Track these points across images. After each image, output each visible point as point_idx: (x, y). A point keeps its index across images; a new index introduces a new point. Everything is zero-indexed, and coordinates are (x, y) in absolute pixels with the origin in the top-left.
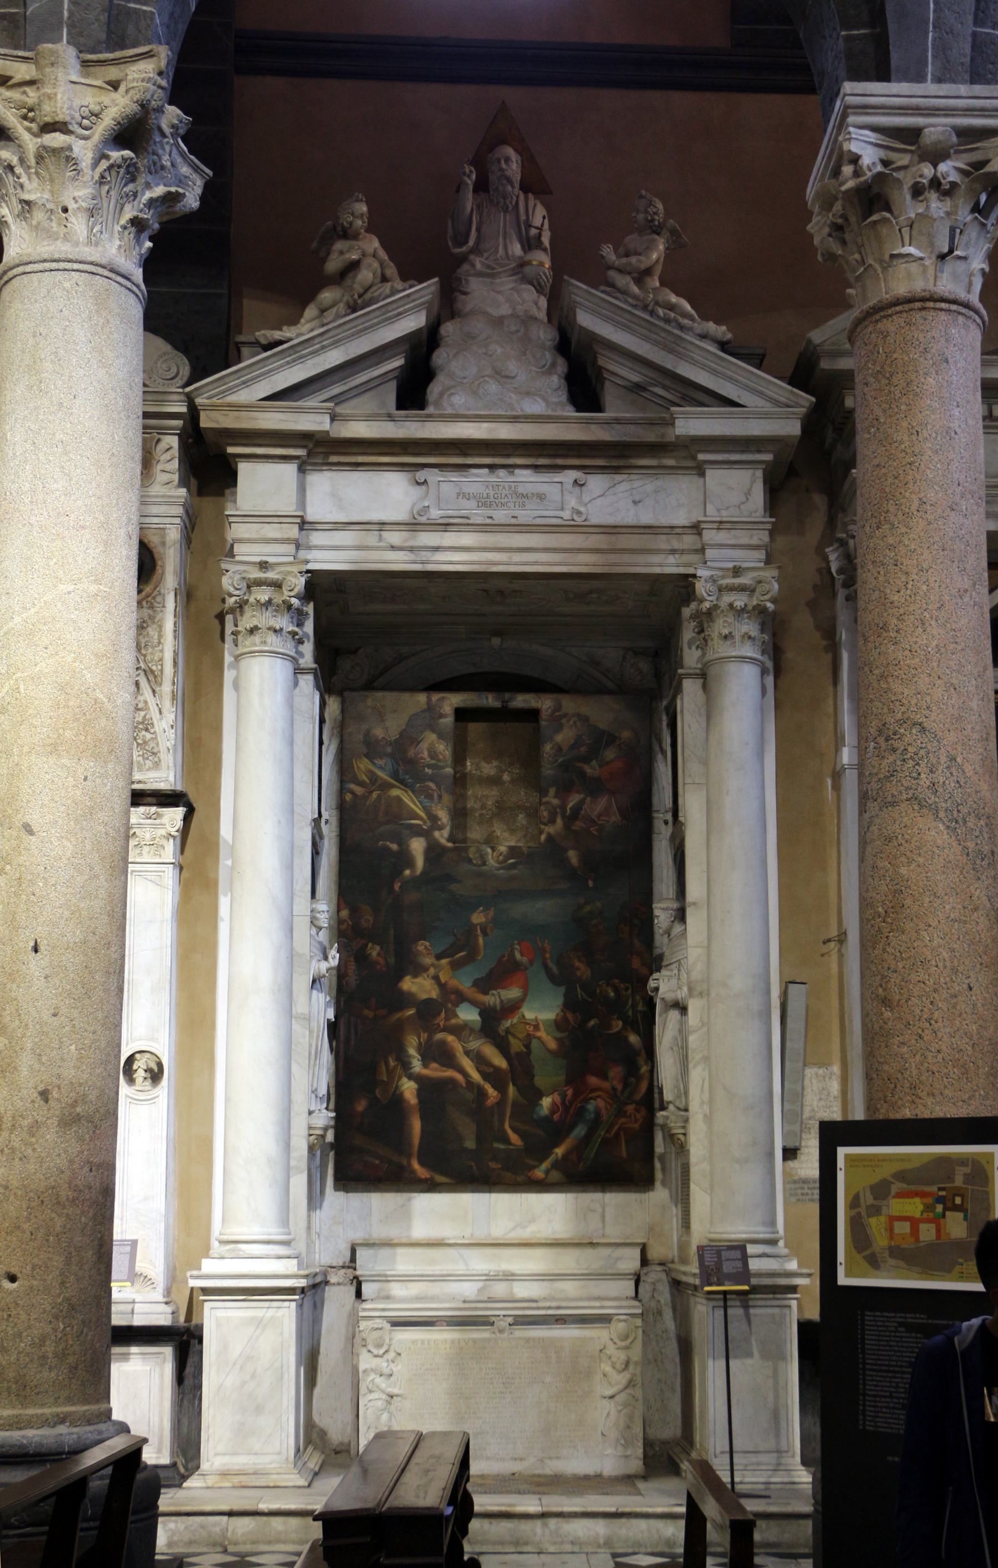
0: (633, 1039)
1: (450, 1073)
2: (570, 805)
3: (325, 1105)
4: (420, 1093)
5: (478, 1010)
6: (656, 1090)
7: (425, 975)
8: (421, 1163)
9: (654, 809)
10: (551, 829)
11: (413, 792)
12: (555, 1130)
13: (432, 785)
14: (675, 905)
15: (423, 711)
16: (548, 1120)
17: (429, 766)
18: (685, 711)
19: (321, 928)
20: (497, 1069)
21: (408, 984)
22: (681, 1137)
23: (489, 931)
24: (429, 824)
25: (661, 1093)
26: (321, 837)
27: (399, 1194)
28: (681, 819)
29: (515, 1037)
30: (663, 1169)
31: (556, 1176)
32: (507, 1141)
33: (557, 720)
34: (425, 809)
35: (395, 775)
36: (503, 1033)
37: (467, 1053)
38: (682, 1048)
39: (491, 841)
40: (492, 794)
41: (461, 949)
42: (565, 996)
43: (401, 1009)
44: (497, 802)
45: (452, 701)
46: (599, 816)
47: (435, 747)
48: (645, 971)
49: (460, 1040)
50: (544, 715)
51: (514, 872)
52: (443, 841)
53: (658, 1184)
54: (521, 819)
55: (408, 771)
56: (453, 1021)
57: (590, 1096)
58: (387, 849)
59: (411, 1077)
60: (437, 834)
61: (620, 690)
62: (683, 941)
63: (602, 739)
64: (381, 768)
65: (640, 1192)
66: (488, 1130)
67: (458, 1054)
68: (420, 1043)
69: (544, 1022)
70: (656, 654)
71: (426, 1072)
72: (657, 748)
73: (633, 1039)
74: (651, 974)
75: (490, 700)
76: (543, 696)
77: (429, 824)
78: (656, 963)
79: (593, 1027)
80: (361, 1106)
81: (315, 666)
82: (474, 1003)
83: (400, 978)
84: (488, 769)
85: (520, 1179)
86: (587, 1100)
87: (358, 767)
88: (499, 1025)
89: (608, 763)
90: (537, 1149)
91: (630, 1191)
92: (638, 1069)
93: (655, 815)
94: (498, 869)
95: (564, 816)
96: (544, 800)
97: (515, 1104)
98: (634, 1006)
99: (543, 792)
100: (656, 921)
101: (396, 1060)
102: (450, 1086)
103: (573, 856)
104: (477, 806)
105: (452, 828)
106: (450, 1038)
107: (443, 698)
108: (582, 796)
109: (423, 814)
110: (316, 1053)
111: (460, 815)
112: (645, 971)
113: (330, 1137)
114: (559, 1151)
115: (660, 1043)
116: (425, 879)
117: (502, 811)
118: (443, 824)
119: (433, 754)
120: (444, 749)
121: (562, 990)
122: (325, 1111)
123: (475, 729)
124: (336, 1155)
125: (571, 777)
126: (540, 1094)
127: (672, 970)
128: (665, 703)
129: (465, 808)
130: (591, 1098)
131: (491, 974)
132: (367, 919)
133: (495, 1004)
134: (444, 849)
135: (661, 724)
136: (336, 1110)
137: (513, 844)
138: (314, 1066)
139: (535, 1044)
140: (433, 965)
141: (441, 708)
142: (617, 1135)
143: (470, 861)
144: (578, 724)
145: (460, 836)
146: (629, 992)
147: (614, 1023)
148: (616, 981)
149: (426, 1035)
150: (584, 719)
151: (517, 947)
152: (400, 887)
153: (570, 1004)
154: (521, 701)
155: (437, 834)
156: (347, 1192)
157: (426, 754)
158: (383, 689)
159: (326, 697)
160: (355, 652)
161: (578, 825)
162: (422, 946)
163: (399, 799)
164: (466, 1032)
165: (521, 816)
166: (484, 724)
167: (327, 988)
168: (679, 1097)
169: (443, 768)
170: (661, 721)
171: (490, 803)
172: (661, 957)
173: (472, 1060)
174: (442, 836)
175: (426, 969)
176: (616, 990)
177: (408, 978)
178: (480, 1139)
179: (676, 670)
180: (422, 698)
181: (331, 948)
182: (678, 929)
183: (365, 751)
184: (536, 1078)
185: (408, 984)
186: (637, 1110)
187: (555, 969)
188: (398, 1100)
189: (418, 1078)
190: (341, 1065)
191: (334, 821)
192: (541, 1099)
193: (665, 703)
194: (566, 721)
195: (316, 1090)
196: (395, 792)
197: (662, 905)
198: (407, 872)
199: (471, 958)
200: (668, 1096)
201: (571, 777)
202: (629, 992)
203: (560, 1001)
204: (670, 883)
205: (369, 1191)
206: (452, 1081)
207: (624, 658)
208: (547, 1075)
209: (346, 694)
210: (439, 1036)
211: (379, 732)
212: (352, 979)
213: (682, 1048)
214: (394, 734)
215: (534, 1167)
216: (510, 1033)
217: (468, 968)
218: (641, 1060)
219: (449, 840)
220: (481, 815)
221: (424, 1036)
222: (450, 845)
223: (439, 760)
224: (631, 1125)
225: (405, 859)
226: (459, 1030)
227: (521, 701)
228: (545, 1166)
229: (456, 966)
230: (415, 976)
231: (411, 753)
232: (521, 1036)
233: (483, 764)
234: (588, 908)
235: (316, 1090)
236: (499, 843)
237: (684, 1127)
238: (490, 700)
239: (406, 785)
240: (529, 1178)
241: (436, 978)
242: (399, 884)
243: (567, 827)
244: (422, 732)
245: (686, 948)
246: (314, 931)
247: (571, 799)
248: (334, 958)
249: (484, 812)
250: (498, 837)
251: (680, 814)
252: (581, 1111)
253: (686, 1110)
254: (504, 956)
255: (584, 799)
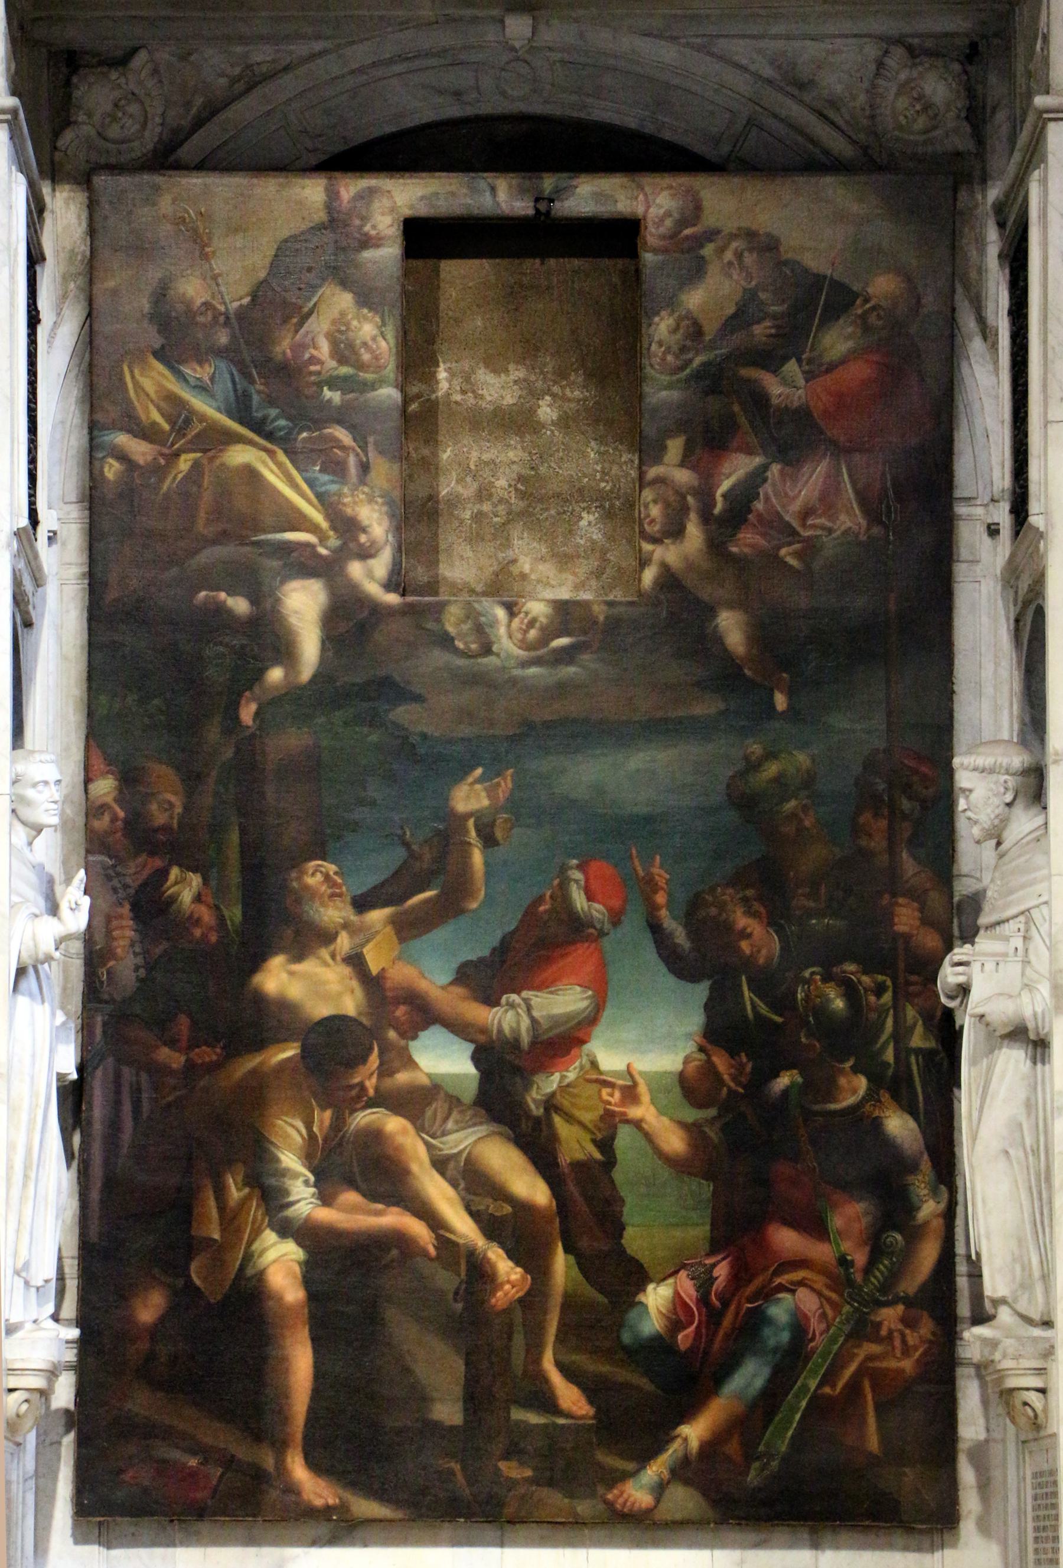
0: (899, 1126)
1: (393, 1218)
2: (725, 486)
3: (50, 1308)
4: (311, 1274)
5: (470, 1048)
6: (962, 1268)
7: (325, 953)
8: (314, 1465)
9: (958, 493)
10: (670, 554)
11: (290, 453)
12: (681, 1375)
13: (342, 435)
14: (1018, 760)
15: (321, 227)
16: (659, 1348)
17: (333, 383)
18: (1053, 215)
19: (38, 829)
20: (523, 1208)
21: (278, 978)
22: (1033, 1398)
23: (499, 834)
24: (334, 542)
25: (976, 1276)
26: (38, 581)
27: (252, 1551)
28: (1035, 520)
29: (569, 1118)
30: (984, 1486)
31: (683, 1500)
32: (547, 1403)
33: (690, 251)
34: (323, 500)
35: (241, 410)
36: (537, 1111)
37: (440, 1164)
38: (1036, 1152)
39: (504, 588)
40: (506, 459)
41: (423, 883)
42: (709, 1007)
43: (260, 1044)
44: (521, 478)
45: (399, 198)
46: (806, 514)
47: (349, 330)
48: (931, 940)
49: (420, 1129)
50: (652, 235)
51: (570, 671)
52: (374, 589)
53: (968, 1527)
54: (589, 525)
55: (276, 396)
56: (403, 1077)
57: (778, 1281)
58: (220, 609)
59: (285, 1230)
60: (356, 569)
61: (871, 159)
62: (1039, 859)
63: (815, 300)
64: (201, 388)
65: (919, 1549)
66: (495, 1381)
67: (415, 1168)
68: (312, 1136)
69: (655, 1080)
70: (972, 54)
71: (325, 1215)
72: (968, 322)
73: (899, 1126)
74: (949, 948)
75: (502, 196)
76: (648, 181)
77: (334, 542)
78: (959, 920)
79: (786, 1092)
80: (149, 1308)
81: (12, 102)
82: (459, 1028)
83: (256, 961)
84: (498, 388)
85: (584, 1508)
86: (768, 1294)
87: (137, 385)
88: (528, 1086)
89: (831, 367)
90: (632, 1425)
91: (891, 1547)
92: (911, 1209)
93: (961, 509)
94: (525, 664)
95: (706, 517)
96: (653, 472)
97: (569, 1303)
98: (900, 1036)
99: (649, 451)
100: (962, 804)
101: (246, 1184)
102: (395, 1252)
103: (732, 628)
104: (468, 491)
105: (399, 550)
106: (394, 1124)
107: (372, 191)
108: (758, 460)
109: (317, 516)
110: (27, 1167)
111: (419, 517)
112: (931, 940)
113: (64, 1395)
114: (693, 1433)
115: (974, 1138)
116: (325, 693)
117: (537, 503)
118: (373, 543)
119: (345, 350)
120: (375, 336)
121: (701, 991)
122: (51, 1324)
123: (460, 276)
124: (81, 1443)
125: (725, 407)
126: (638, 1276)
127: (1007, 939)
128: (993, 193)
129: (433, 498)
130: (781, 1288)
131: (503, 949)
132: (167, 804)
133: (516, 1031)
134: (377, 611)
135: (982, 251)
136: (81, 1322)
137: (564, 594)
138: (22, 1199)
139: (624, 1138)
140: (346, 926)
141: (364, 219)
142: (854, 1387)
143: (446, 641)
144: (749, 259)
145: (421, 574)
146: (887, 997)
147: (843, 1081)
148: (851, 967)
149: (328, 1114)
150: (766, 246)
151: (577, 875)
152: (257, 714)
153: (722, 1031)
154: (588, 196)
155: (356, 569)
156: (109, 1547)
157: (324, 349)
158: (202, 166)
159: (46, 190)
160: (122, 61)
161: (747, 541)
162: (316, 875)
163: (251, 474)
164: (439, 1106)
165: (587, 518)
166: (486, 263)
167: (57, 990)
168: (1025, 1286)
169: (373, 386)
170: (981, 244)
171: (502, 483)
172: (975, 902)
173: (454, 1184)
174: (370, 576)
175: (327, 937)
176: (850, 991)
177: (277, 962)
178: (474, 1399)
179: (1029, 96)
180: (312, 191)
181: (68, 881)
182: (1023, 823)
183: (157, 341)
184: (629, 1232)
185: (278, 978)
186: (909, 1322)
187: (680, 936)
188: (249, 1294)
189: (306, 1234)
190: (95, 1195)
191: (73, 536)
192: (641, 1288)
193: (993, 193)
194: (714, 247)
195: (26, 1266)
196: (240, 456)
197: (981, 761)
198: (276, 674)
199: (450, 906)
200: (994, 1284)
201: (725, 407)
202: (887, 997)
203: (694, 1021)
204: (1004, 700)
205: (171, 1544)
206: (399, 1239)
207: (880, 65)
208: (660, 1223)
209: (100, 180)
210: (363, 1118)
211: (192, 289)
212: (126, 967)
213: (1036, 1152)
214: (235, 295)
215: (626, 1476)
216: (558, 1109)
217: (441, 934)
218: (921, 1185)
219: (389, 586)
220: (478, 517)
221: (323, 1118)
222: (392, 599)
223: (361, 366)
224: (893, 1364)
225: (268, 637)
226: (418, 1102)
227: (588, 196)
228: (655, 1471)
229: (408, 928)
230: (299, 957)
231: (283, 346)
232: (588, 1117)
233: (483, 375)
234: (772, 769)
235: (26, 1266)
236: (528, 585)
237: (1041, 1371)
238: (502, 196)
239: (269, 436)
240: (610, 1505)
241: (356, 961)
242: (253, 707)
243: (716, 546)
244: (314, 288)
245: (1049, 877)
246: (21, 834)
247: (726, 467)
248: (76, 911)
249: (486, 507)
250: (524, 577)
251: (1034, 507)
252: (753, 1324)
253: (1048, 1324)
254: (540, 900)
255: (765, 467)
